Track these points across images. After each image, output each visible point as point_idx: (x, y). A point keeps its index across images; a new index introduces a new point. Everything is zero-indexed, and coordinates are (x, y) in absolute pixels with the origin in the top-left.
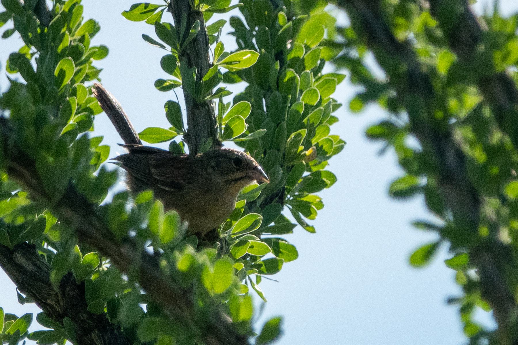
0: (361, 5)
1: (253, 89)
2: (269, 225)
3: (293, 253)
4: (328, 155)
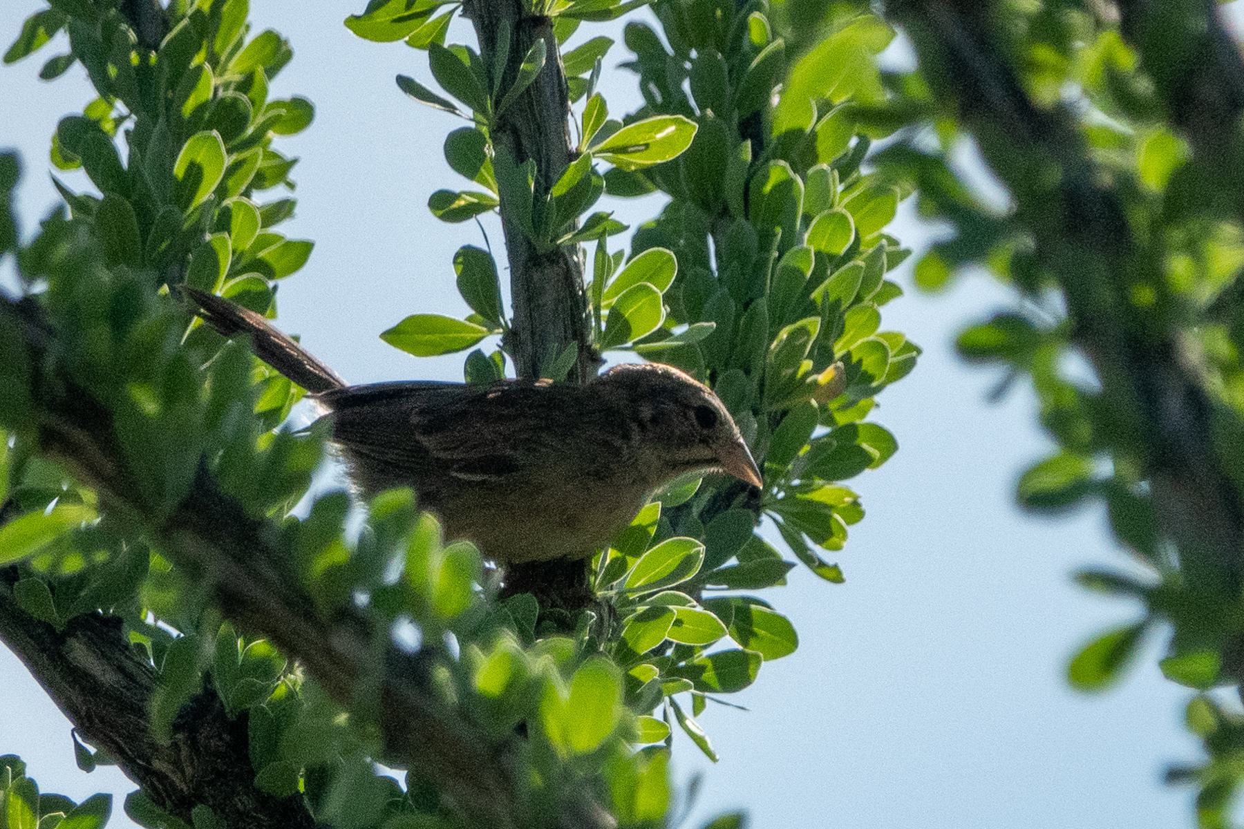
0: (943, 14)
1: (683, 213)
2: (723, 566)
3: (785, 637)
4: (874, 384)
